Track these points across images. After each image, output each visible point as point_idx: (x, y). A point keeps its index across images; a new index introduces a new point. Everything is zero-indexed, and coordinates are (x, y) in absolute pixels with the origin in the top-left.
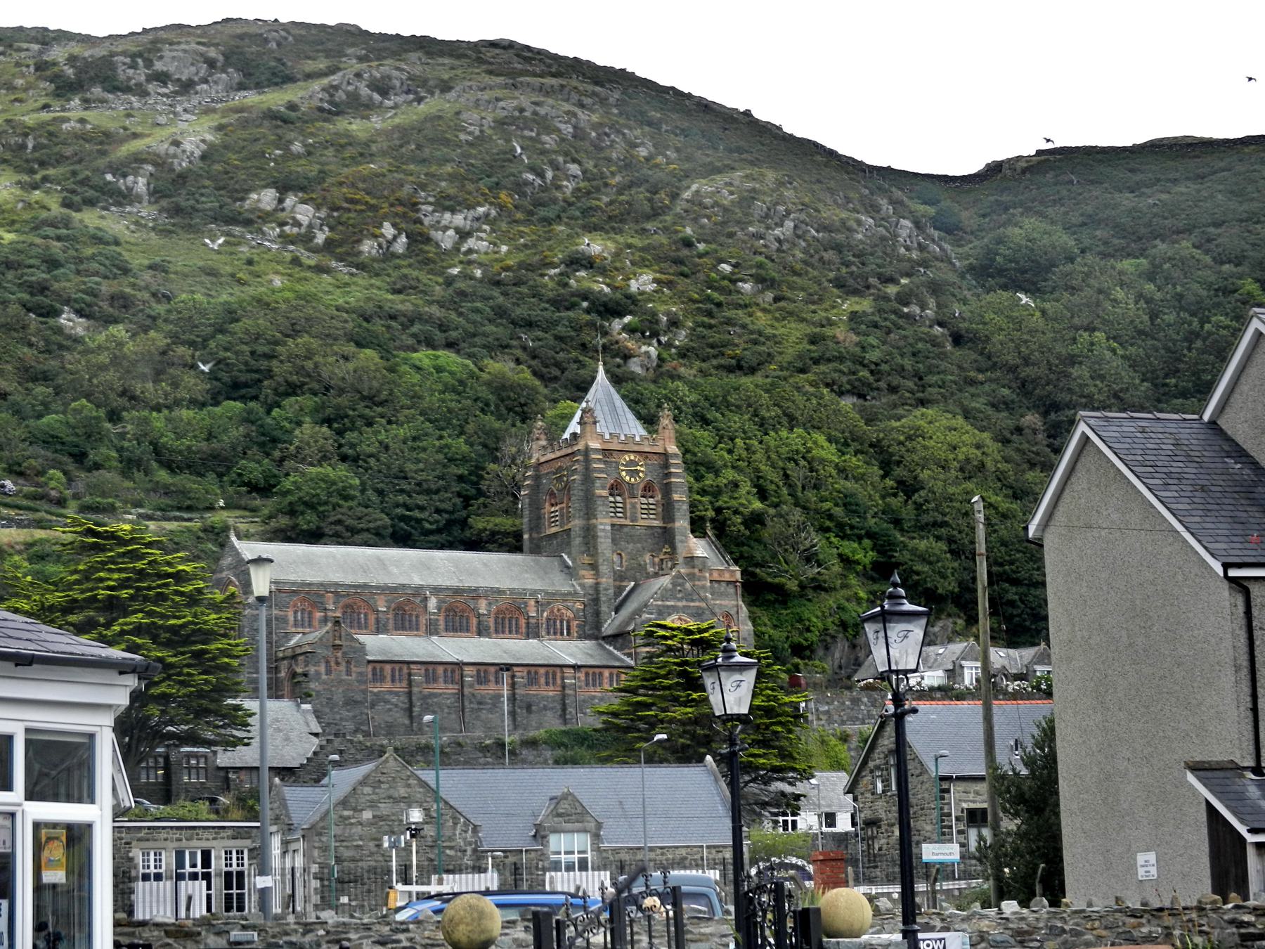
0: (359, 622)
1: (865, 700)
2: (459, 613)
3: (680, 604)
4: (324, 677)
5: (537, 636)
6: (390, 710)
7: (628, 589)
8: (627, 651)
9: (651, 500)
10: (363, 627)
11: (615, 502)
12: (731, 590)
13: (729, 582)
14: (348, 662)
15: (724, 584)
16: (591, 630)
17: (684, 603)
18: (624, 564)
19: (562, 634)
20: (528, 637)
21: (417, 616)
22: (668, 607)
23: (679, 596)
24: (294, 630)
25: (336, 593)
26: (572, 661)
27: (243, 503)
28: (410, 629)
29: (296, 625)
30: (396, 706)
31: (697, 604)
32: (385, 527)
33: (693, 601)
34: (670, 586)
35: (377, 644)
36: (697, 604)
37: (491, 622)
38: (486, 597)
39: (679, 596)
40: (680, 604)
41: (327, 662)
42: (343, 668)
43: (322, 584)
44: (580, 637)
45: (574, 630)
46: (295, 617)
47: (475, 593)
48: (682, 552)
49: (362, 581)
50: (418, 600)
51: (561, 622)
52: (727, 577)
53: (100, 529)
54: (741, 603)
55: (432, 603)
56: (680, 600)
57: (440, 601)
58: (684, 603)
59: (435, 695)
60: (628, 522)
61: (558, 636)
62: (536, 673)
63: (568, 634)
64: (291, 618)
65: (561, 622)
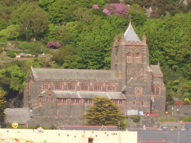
0: (83, 88)
3: (139, 84)
4: (46, 102)
5: (105, 91)
6: (63, 109)
9: (139, 57)
11: (129, 58)
12: (160, 79)
14: (52, 98)
15: (56, 104)
16: (119, 89)
19: (112, 90)
21: (74, 86)
24: (43, 90)
26: (80, 97)
27: (152, 106)
28: (85, 89)
29: (44, 88)
30: (64, 108)
37: (93, 88)
40: (139, 84)
41: (47, 98)
42: (51, 100)
46: (44, 87)
48: (145, 70)
50: (74, 83)
51: (112, 87)
56: (139, 83)
58: (140, 84)
59: (74, 106)
61: (111, 91)
63: (114, 90)
65: (112, 87)
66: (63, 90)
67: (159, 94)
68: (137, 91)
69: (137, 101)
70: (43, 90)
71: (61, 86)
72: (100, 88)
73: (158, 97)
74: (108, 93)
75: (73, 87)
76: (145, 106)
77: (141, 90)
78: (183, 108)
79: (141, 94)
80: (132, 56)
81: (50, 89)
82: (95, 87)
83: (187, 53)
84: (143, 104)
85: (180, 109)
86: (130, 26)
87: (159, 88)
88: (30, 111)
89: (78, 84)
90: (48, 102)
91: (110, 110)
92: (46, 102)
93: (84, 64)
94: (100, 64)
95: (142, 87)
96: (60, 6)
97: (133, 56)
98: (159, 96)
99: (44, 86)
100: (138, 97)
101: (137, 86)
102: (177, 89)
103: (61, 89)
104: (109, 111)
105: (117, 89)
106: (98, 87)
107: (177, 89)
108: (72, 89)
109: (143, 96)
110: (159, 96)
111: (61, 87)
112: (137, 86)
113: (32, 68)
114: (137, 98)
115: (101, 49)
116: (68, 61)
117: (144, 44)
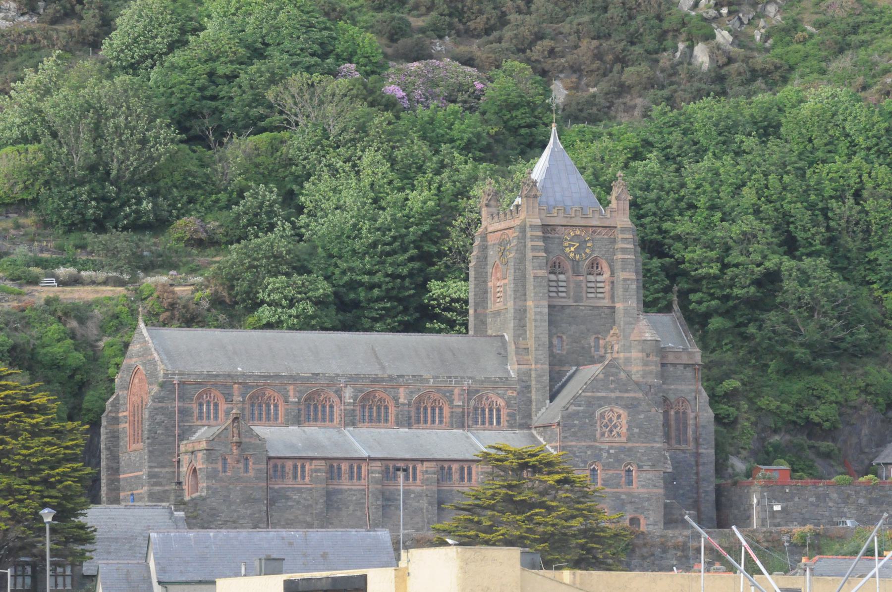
1: (835, 496)
2: (370, 404)
3: (613, 395)
4: (221, 475)
7: (568, 374)
8: (554, 444)
10: (271, 419)
11: (557, 281)
12: (689, 373)
13: (686, 366)
15: (681, 368)
17: (618, 394)
18: (565, 347)
19: (491, 423)
20: (452, 427)
22: (599, 398)
23: (612, 386)
25: (244, 385)
26: (365, 454)
31: (632, 395)
32: (326, 296)
33: (627, 391)
34: (601, 376)
35: (280, 437)
36: (632, 395)
38: (407, 385)
39: (612, 386)
43: (229, 375)
44: (511, 427)
45: (504, 418)
47: (394, 381)
49: (272, 372)
51: (491, 410)
52: (685, 359)
53: (49, 438)
54: (701, 387)
55: (348, 394)
56: (612, 391)
57: (357, 391)
58: (618, 394)
60: (570, 302)
62: (450, 468)
63: (499, 422)
64: (196, 411)
65: (491, 410)
66: (287, 424)
67: (686, 441)
68: (606, 426)
69: (607, 466)
70: (199, 423)
71: (276, 406)
72: (441, 413)
73: (683, 451)
74: (478, 438)
75: (324, 411)
76: (642, 490)
77: (624, 421)
78: (796, 499)
79: (624, 439)
80: (570, 272)
81: (236, 419)
82: (418, 409)
83: (767, 264)
84: (630, 483)
85: (785, 504)
86: (555, 142)
87: (684, 413)
88: (176, 514)
89: (348, 394)
90: (229, 474)
91: (565, 501)
92: (221, 475)
93: (345, 311)
94: (405, 311)
95: (626, 407)
96: (202, 68)
97: (576, 273)
98: (683, 446)
99: (201, 405)
100: (612, 451)
101: (606, 401)
102: (736, 418)
103: (276, 419)
104: (563, 509)
105: (511, 416)
106: (433, 409)
107: (736, 418)
108: (324, 420)
109: (630, 445)
110: (683, 446)
111: (276, 410)
112: (606, 401)
113: (142, 325)
114: (605, 455)
115: (413, 252)
116: (276, 296)
117: (623, 220)
